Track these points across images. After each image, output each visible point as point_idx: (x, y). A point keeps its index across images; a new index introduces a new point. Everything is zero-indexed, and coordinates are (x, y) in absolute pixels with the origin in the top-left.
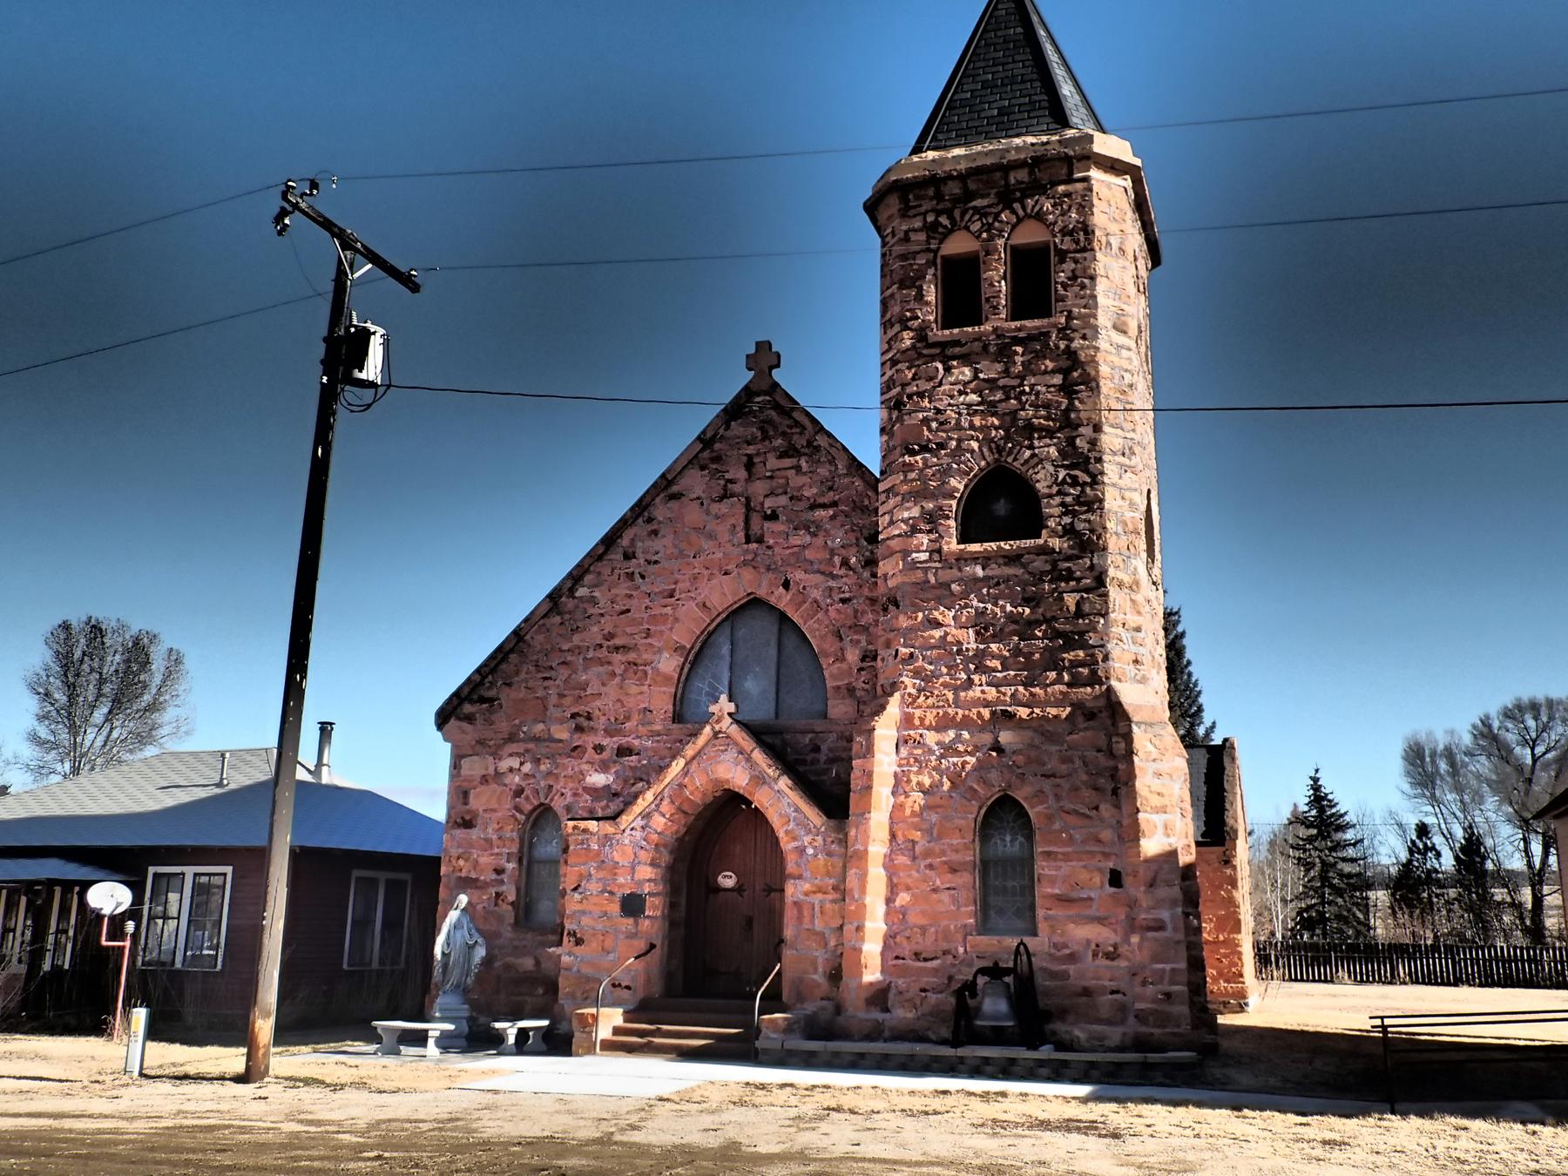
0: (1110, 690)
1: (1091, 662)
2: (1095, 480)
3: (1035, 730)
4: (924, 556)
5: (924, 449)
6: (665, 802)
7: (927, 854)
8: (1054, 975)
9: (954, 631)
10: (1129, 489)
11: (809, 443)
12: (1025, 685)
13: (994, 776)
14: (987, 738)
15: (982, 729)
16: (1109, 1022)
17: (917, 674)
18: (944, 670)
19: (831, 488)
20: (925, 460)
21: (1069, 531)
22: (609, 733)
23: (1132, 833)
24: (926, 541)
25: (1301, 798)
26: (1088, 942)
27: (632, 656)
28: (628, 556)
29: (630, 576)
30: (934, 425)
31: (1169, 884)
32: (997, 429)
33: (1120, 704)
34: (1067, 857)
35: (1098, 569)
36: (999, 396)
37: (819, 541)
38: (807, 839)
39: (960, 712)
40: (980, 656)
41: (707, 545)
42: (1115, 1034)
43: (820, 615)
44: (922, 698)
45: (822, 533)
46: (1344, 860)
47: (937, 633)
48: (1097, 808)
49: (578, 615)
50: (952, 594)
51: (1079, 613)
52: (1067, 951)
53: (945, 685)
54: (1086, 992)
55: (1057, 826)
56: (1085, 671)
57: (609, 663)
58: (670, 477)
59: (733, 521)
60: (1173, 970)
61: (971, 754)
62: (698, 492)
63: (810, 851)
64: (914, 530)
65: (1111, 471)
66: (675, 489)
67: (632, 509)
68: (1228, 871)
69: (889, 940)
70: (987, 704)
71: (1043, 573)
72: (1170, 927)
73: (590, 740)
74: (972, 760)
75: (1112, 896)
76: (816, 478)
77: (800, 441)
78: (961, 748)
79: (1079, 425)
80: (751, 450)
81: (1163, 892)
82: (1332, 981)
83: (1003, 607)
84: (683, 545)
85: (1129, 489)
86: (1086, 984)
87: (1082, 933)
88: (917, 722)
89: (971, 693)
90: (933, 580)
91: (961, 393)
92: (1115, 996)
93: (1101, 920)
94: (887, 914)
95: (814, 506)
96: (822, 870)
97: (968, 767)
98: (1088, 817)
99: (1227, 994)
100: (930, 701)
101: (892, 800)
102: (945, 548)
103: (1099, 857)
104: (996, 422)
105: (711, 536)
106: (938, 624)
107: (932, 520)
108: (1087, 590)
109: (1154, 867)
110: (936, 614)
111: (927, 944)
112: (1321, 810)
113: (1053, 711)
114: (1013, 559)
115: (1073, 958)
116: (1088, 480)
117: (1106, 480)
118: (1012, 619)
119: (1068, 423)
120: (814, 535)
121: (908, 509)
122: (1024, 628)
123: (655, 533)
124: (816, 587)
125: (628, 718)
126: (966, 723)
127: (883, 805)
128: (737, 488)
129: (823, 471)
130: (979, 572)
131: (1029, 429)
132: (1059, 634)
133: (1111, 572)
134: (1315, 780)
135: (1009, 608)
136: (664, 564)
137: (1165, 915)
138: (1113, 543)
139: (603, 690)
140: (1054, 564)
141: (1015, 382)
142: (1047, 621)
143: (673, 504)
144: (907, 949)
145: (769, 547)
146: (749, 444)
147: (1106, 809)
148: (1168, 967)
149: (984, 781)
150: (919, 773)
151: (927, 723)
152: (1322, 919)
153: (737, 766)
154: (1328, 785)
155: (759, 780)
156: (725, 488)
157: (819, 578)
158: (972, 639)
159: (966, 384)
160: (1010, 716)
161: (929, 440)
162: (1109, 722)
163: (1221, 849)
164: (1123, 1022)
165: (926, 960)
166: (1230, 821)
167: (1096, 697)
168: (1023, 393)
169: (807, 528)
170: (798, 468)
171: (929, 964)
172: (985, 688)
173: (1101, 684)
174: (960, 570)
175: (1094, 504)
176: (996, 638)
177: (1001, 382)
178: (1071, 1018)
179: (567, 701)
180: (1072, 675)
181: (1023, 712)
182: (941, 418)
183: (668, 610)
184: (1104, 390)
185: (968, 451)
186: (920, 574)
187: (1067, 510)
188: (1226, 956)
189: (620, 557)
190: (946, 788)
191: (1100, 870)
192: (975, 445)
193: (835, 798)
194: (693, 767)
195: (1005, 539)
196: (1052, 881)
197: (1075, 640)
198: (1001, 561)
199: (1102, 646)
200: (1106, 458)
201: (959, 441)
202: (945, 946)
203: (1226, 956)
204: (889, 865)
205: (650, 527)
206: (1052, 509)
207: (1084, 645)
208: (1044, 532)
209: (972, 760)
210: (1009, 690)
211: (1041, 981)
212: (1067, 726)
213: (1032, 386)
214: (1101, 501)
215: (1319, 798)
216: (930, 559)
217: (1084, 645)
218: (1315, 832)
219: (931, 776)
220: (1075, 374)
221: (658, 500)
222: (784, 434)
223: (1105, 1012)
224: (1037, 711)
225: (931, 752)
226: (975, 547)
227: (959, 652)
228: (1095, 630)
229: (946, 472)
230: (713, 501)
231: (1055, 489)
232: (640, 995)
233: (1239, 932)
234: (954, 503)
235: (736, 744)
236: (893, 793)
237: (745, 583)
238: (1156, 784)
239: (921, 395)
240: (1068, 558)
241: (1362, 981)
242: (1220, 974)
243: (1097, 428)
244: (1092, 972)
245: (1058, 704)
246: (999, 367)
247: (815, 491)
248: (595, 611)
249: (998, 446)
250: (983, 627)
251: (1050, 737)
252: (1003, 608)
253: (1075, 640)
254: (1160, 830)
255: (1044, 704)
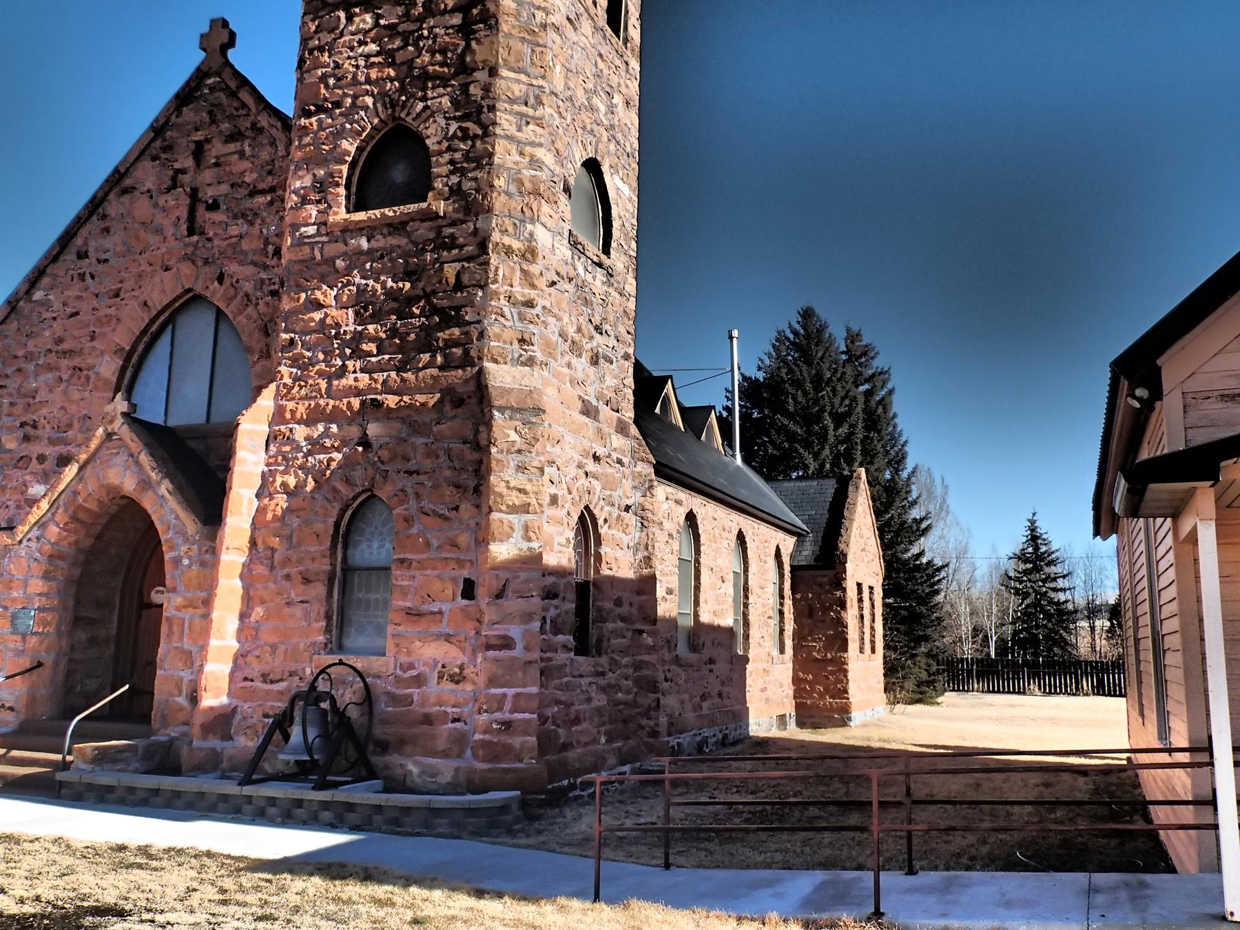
0: (481, 372)
1: (464, 342)
2: (487, 131)
3: (403, 421)
4: (311, 230)
5: (320, 109)
6: (60, 511)
7: (287, 561)
8: (393, 699)
9: (334, 312)
10: (532, 144)
11: (254, 125)
12: (399, 370)
13: (358, 474)
14: (354, 432)
15: (351, 421)
16: (445, 755)
17: (295, 362)
18: (321, 356)
19: (270, 173)
20: (320, 122)
21: (456, 192)
22: (52, 442)
23: (482, 538)
24: (314, 213)
25: (1016, 540)
26: (436, 662)
27: (77, 361)
28: (82, 255)
29: (82, 277)
30: (332, 81)
31: (570, 601)
32: (392, 80)
33: (487, 386)
34: (422, 565)
35: (481, 234)
36: (398, 43)
37: (256, 230)
38: (184, 548)
39: (331, 402)
40: (359, 337)
41: (153, 239)
42: (446, 769)
43: (250, 310)
44: (296, 389)
45: (259, 221)
46: (1055, 590)
47: (317, 316)
48: (456, 508)
49: (35, 316)
50: (337, 271)
51: (459, 286)
52: (414, 673)
53: (320, 374)
54: (428, 720)
55: (414, 531)
56: (458, 351)
57: (58, 369)
58: (122, 170)
59: (178, 214)
60: (517, 695)
61: (338, 450)
62: (149, 184)
63: (186, 562)
64: (304, 201)
65: (505, 121)
66: (127, 182)
67: (86, 206)
68: (838, 593)
69: (240, 659)
70: (358, 393)
71: (427, 241)
72: (520, 646)
73: (35, 449)
74: (338, 456)
75: (463, 609)
76: (257, 162)
77: (245, 124)
78: (328, 443)
79: (474, 70)
80: (198, 136)
81: (512, 604)
82: (1024, 693)
83: (384, 282)
84: (133, 242)
85: (532, 144)
86: (427, 710)
87: (431, 653)
88: (288, 416)
89: (344, 381)
90: (318, 257)
91: (361, 43)
92: (458, 725)
93: (448, 638)
94: (240, 631)
95: (253, 193)
96: (194, 582)
97: (334, 465)
98: (446, 519)
99: (832, 709)
100: (303, 392)
101: (256, 503)
102: (331, 219)
103: (453, 565)
104: (392, 73)
105: (159, 231)
106: (319, 306)
107: (322, 188)
108: (469, 259)
109: (504, 575)
110: (318, 294)
111: (276, 664)
112: (1036, 548)
113: (421, 398)
114: (397, 227)
115: (419, 681)
116: (480, 132)
117: (498, 131)
118: (390, 294)
119: (464, 69)
120: (251, 224)
121: (301, 178)
122: (401, 304)
123: (107, 230)
124: (247, 279)
125: (70, 426)
126: (333, 416)
127: (244, 509)
128: (185, 179)
129: (265, 155)
130: (364, 244)
131: (425, 76)
132: (436, 310)
133: (496, 236)
134: (1033, 522)
135: (390, 283)
136: (113, 262)
137: (515, 631)
138: (499, 202)
139: (51, 397)
140: (439, 230)
141: (413, 27)
142: (427, 296)
143: (126, 199)
144: (256, 669)
145: (209, 240)
146: (197, 130)
147: (466, 509)
148: (511, 692)
149: (348, 481)
150: (284, 473)
151: (298, 416)
152: (1034, 640)
153: (132, 473)
154: (1043, 527)
155: (145, 484)
156: (174, 179)
157: (250, 270)
158: (351, 320)
159: (366, 32)
160: (377, 404)
161: (326, 100)
162: (477, 410)
163: (831, 573)
164: (460, 755)
165: (272, 682)
166: (842, 546)
167: (466, 381)
168: (421, 37)
169: (244, 216)
170: (241, 154)
171: (276, 687)
172: (359, 375)
173: (473, 365)
174: (346, 244)
175: (483, 160)
176: (376, 318)
177: (401, 28)
178: (408, 749)
179: (18, 409)
180: (445, 357)
181: (391, 401)
182: (339, 73)
183: (112, 311)
184: (504, 27)
185: (362, 108)
186: (307, 250)
187: (455, 167)
188: (832, 673)
189: (74, 257)
190: (309, 489)
191: (454, 580)
192: (369, 101)
193: (208, 500)
194: (88, 471)
195: (389, 205)
196: (404, 593)
197: (451, 317)
198: (385, 231)
199: (479, 322)
200: (501, 105)
201: (355, 97)
202: (293, 666)
203: (832, 673)
204: (246, 576)
205: (103, 225)
206: (440, 168)
207: (460, 322)
208: (430, 194)
209: (338, 456)
210: (380, 377)
211: (384, 707)
212: (434, 416)
213: (431, 29)
214: (491, 155)
215: (1034, 538)
216: (318, 233)
217: (460, 322)
218: (1029, 566)
219: (296, 476)
220: (475, 11)
221: (111, 196)
222: (231, 118)
223: (441, 744)
224: (406, 398)
225: (298, 448)
226: (361, 216)
227: (337, 336)
228: (471, 304)
229: (339, 134)
230: (162, 193)
231: (445, 144)
232: (22, 717)
233: (846, 651)
234: (345, 169)
235: (127, 447)
236: (258, 496)
237: (186, 276)
238: (518, 480)
239: (321, 49)
240: (453, 224)
241: (1050, 693)
242: (827, 691)
243: (493, 72)
244: (437, 695)
245: (429, 390)
246: (400, 10)
247: (255, 175)
248: (49, 315)
249: (391, 100)
250: (363, 306)
251: (416, 428)
252: (384, 284)
253: (451, 317)
254: (518, 534)
255: (411, 391)
